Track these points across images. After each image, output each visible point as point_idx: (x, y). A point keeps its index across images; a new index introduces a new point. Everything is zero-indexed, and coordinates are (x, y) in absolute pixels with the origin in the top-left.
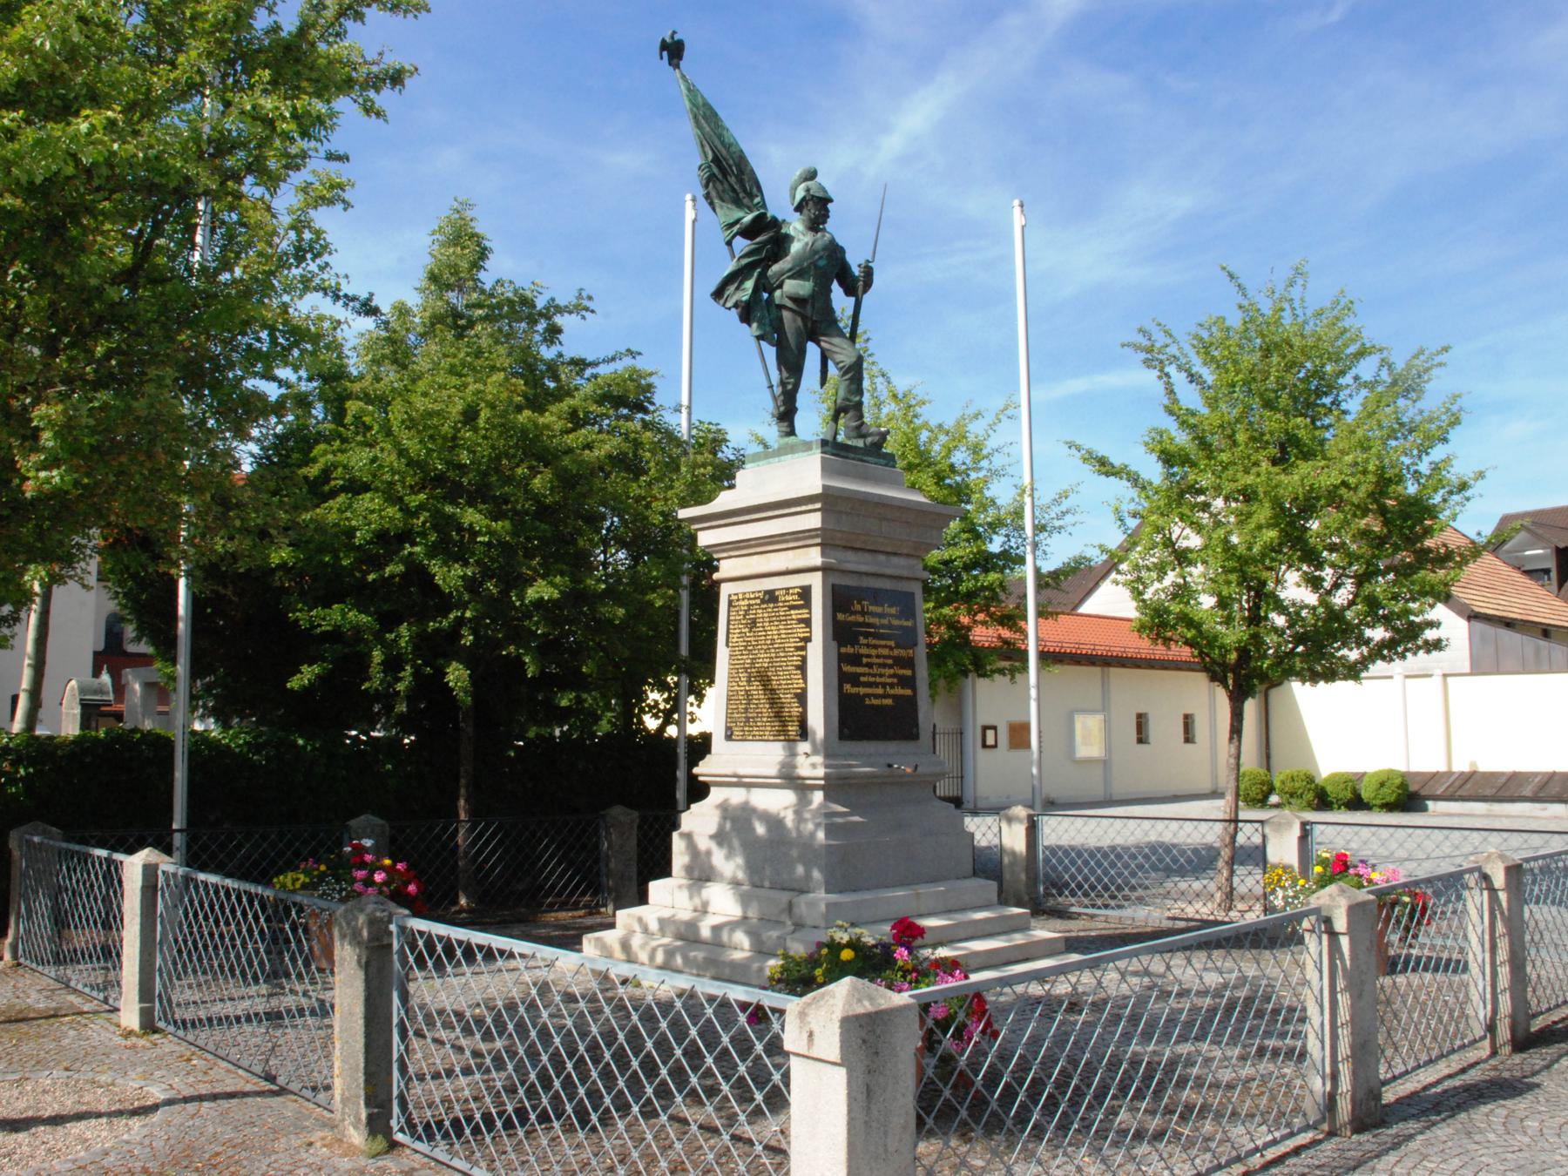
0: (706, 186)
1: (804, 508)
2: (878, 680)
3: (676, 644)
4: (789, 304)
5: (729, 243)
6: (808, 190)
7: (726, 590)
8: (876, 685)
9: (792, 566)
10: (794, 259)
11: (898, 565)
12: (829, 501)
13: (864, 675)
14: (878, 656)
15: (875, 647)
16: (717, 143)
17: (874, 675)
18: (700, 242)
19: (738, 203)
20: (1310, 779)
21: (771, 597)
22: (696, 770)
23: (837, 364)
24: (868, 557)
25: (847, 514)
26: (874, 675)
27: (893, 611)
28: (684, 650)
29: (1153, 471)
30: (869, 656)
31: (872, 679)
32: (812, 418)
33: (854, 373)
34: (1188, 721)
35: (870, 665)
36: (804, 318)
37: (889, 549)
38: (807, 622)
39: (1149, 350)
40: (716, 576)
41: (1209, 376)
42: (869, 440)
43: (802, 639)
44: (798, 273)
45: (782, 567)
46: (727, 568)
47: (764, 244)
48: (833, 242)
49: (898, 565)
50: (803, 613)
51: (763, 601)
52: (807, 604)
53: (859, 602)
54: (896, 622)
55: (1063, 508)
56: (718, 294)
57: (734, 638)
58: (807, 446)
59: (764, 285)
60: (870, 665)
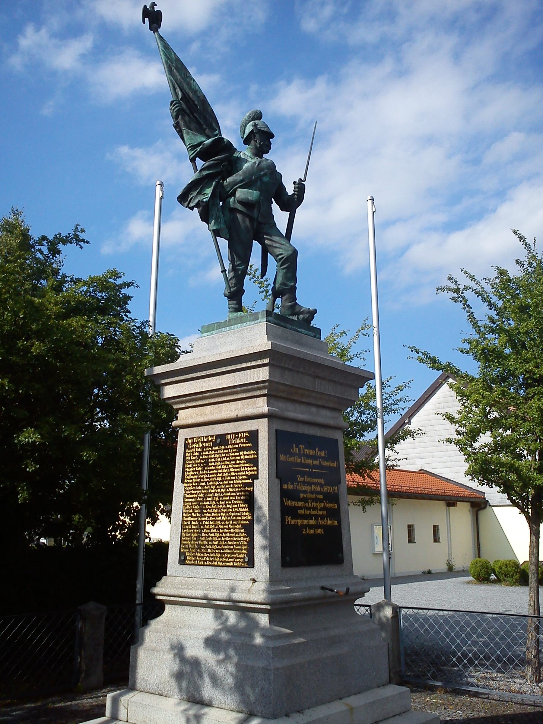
0: (176, 118)
1: (253, 363)
2: (312, 512)
3: (140, 482)
4: (239, 207)
5: (193, 160)
6: (255, 125)
7: (183, 435)
8: (310, 517)
9: (241, 414)
10: (244, 173)
11: (325, 417)
12: (274, 357)
13: (301, 508)
14: (312, 492)
15: (310, 484)
16: (185, 86)
17: (309, 509)
18: (172, 163)
19: (201, 130)
20: (516, 565)
21: (222, 440)
22: (156, 590)
23: (276, 256)
24: (304, 408)
25: (290, 370)
26: (309, 509)
27: (322, 454)
28: (145, 486)
29: (472, 367)
30: (305, 492)
31: (307, 512)
32: (254, 296)
33: (290, 263)
34: (436, 529)
35: (305, 500)
36: (251, 219)
37: (320, 403)
38: (255, 462)
39: (457, 291)
40: (174, 423)
41: (500, 304)
42: (301, 316)
43: (249, 477)
44: (247, 184)
45: (232, 414)
46: (184, 416)
47: (220, 161)
48: (272, 167)
49: (325, 417)
50: (251, 455)
51: (215, 444)
52: (255, 447)
53: (297, 446)
54: (325, 464)
55: (398, 397)
56: (183, 198)
57: (189, 476)
58: (255, 317)
59: (222, 194)
60: (305, 500)
